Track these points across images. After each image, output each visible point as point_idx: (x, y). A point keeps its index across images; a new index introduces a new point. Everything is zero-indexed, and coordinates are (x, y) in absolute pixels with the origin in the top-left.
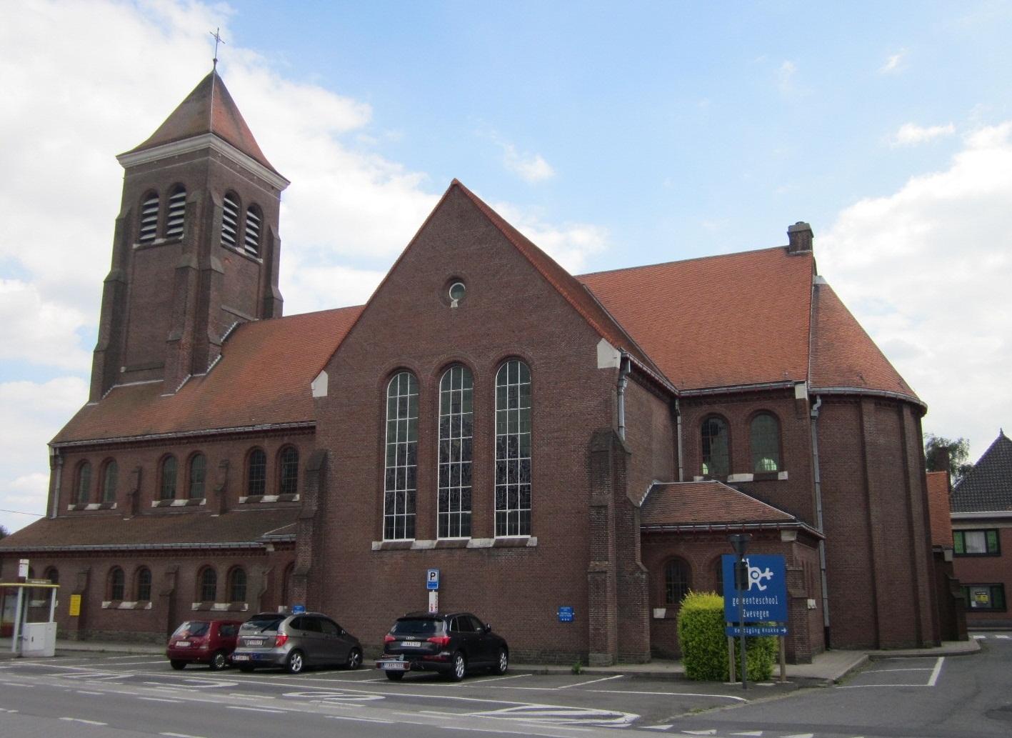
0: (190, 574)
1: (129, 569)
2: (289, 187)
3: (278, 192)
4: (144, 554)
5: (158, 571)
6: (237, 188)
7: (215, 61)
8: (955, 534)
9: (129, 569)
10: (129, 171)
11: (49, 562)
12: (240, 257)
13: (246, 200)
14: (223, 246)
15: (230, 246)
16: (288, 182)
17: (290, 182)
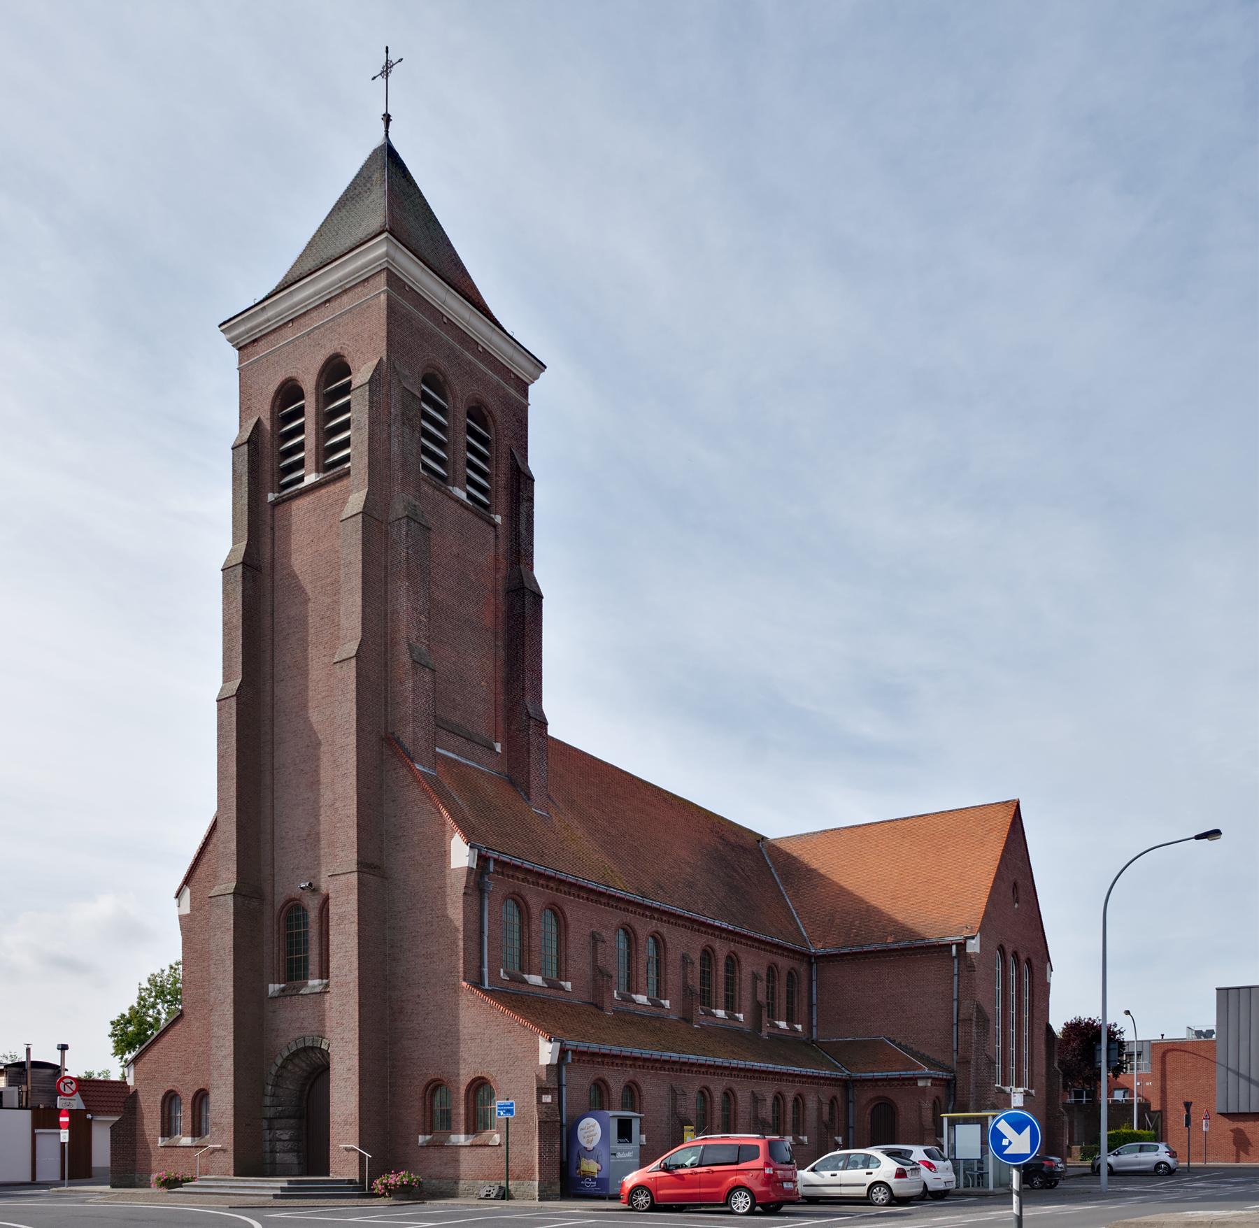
3: (523, 388)
7: (387, 118)
11: (631, 1074)
13: (461, 393)
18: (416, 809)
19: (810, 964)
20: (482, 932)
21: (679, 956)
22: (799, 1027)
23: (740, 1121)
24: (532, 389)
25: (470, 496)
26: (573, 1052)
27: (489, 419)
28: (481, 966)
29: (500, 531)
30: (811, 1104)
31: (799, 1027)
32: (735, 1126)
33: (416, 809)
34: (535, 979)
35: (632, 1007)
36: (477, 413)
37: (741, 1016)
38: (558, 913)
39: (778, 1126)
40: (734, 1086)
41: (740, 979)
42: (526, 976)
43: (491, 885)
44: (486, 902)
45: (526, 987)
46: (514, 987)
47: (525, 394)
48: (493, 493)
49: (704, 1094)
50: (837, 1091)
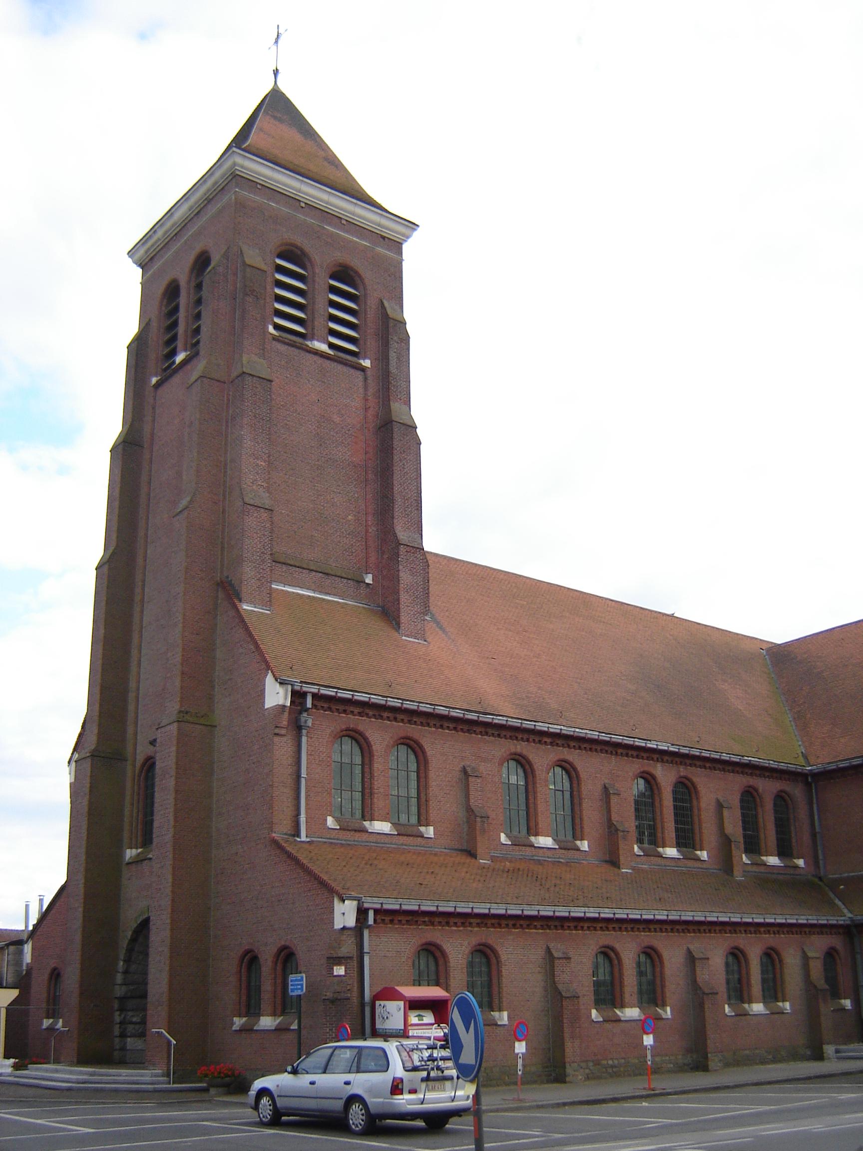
0: (715, 956)
1: (629, 950)
2: (415, 234)
3: (397, 247)
4: (652, 927)
5: (519, 958)
6: (356, 263)
7: (276, 72)
8: (362, 1067)
9: (629, 950)
10: (144, 265)
11: (770, 940)
12: (316, 358)
13: (322, 260)
14: (275, 338)
15: (298, 340)
16: (413, 226)
17: (418, 226)
18: (241, 650)
19: (808, 785)
20: (299, 777)
21: (599, 788)
22: (801, 862)
23: (627, 997)
24: (405, 247)
25: (331, 346)
26: (377, 911)
27: (357, 279)
28: (298, 814)
29: (369, 373)
30: (791, 960)
31: (801, 862)
32: (500, 1002)
33: (241, 650)
34: (545, 841)
35: (528, 851)
36: (344, 273)
37: (704, 855)
38: (414, 746)
39: (741, 991)
40: (656, 943)
41: (699, 810)
42: (660, 850)
43: (308, 720)
44: (304, 739)
45: (364, 836)
46: (518, 852)
47: (400, 252)
48: (361, 342)
49: (737, 956)
50: (836, 941)
